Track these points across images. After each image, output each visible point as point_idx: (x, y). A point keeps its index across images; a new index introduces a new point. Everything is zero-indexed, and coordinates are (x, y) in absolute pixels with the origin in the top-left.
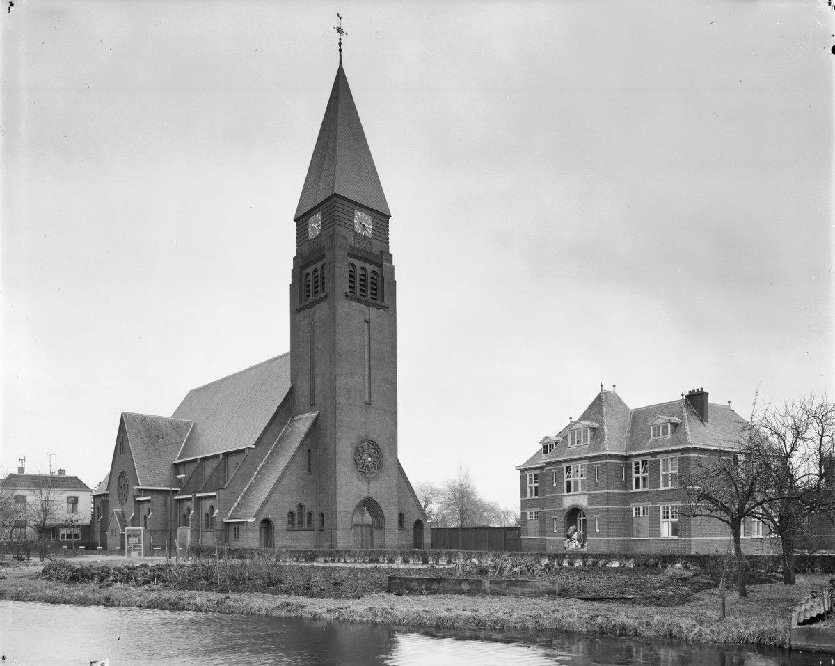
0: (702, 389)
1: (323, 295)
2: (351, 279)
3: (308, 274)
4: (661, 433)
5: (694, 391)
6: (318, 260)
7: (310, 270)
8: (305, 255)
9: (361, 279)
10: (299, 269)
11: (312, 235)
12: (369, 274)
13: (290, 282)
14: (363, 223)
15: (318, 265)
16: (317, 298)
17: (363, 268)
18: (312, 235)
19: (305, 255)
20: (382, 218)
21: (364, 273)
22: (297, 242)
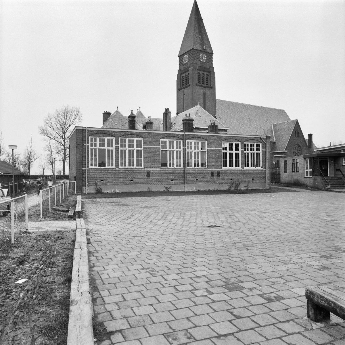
0: (110, 112)
1: (188, 85)
2: (199, 78)
3: (183, 76)
4: (86, 166)
5: (108, 112)
6: (185, 72)
7: (184, 75)
8: (182, 70)
9: (202, 78)
10: (180, 74)
11: (184, 62)
12: (201, 75)
13: (176, 79)
14: (203, 57)
15: (187, 73)
16: (186, 86)
17: (203, 74)
18: (184, 62)
19: (182, 70)
20: (210, 54)
21: (203, 75)
22: (179, 65)
